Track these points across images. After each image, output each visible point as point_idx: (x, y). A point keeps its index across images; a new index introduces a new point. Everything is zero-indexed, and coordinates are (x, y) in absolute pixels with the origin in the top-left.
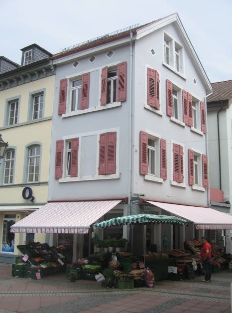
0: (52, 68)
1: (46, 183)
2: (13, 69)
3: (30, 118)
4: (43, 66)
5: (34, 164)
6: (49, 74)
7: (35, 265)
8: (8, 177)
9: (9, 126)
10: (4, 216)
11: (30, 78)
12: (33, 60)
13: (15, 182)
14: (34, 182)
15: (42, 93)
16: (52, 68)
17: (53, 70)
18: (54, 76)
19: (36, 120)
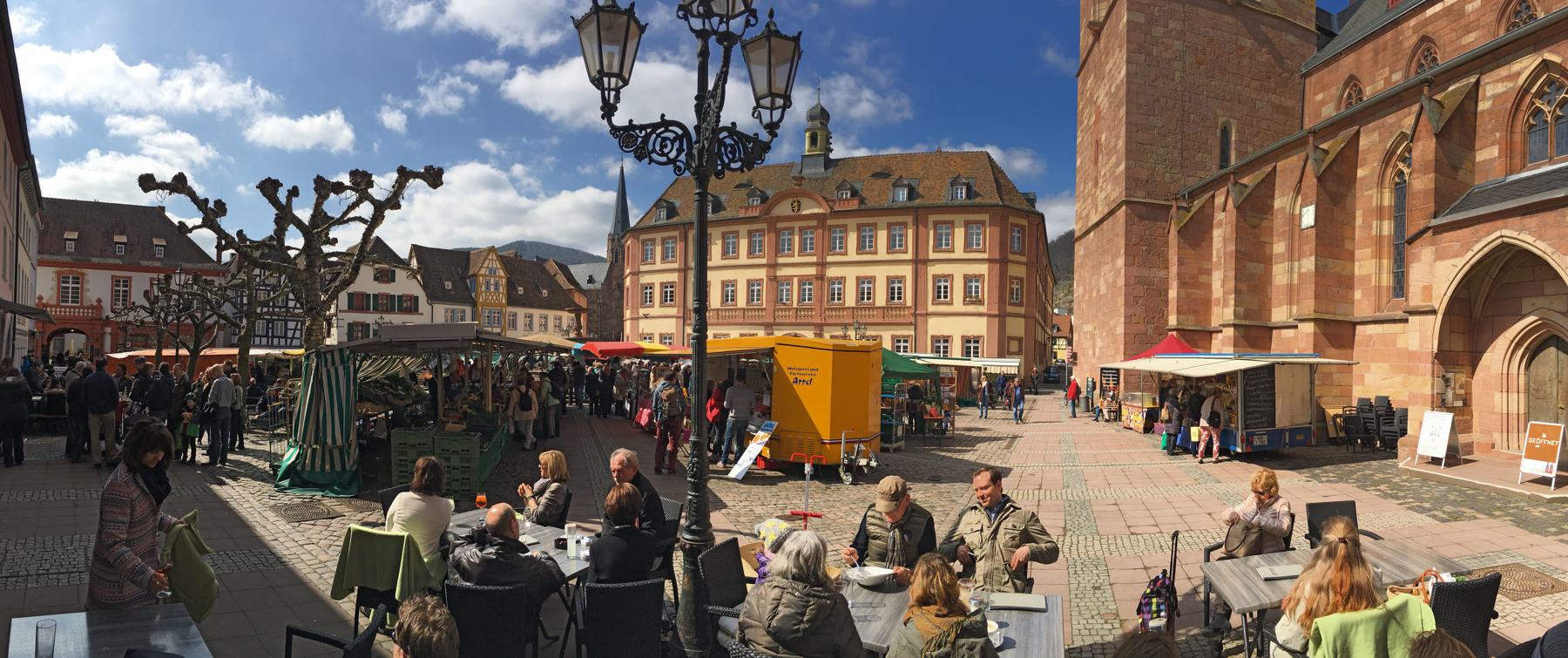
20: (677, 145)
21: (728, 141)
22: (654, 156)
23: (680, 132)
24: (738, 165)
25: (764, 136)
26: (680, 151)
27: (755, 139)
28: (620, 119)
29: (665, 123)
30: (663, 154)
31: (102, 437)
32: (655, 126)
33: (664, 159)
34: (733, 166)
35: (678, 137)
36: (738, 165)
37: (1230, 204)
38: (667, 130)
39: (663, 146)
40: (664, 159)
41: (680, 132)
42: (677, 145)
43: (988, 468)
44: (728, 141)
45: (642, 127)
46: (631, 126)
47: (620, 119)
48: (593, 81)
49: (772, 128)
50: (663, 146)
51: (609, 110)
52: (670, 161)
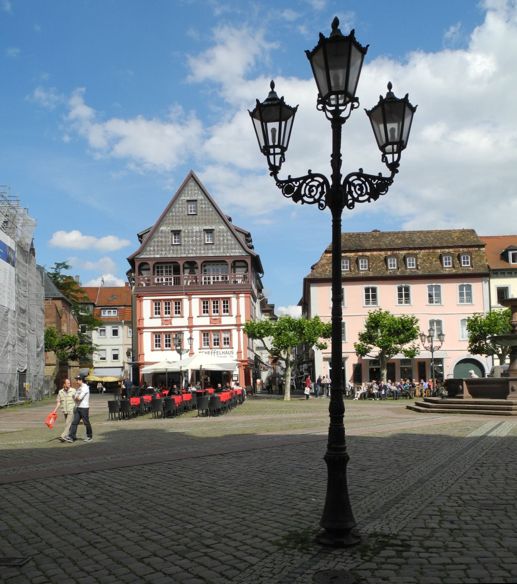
20: (320, 189)
21: (356, 182)
22: (305, 198)
23: (321, 180)
24: (366, 197)
25: (387, 173)
26: (322, 193)
27: (380, 177)
28: (282, 176)
29: (311, 176)
30: (311, 197)
31: (111, 458)
32: (305, 179)
33: (311, 200)
34: (361, 199)
35: (321, 185)
36: (366, 197)
37: (140, 456)
38: (313, 180)
39: (310, 191)
40: (311, 200)
41: (321, 180)
42: (320, 189)
43: (417, 397)
44: (356, 182)
45: (297, 180)
46: (290, 180)
47: (282, 176)
48: (262, 151)
49: (394, 167)
50: (310, 191)
51: (274, 170)
52: (315, 201)
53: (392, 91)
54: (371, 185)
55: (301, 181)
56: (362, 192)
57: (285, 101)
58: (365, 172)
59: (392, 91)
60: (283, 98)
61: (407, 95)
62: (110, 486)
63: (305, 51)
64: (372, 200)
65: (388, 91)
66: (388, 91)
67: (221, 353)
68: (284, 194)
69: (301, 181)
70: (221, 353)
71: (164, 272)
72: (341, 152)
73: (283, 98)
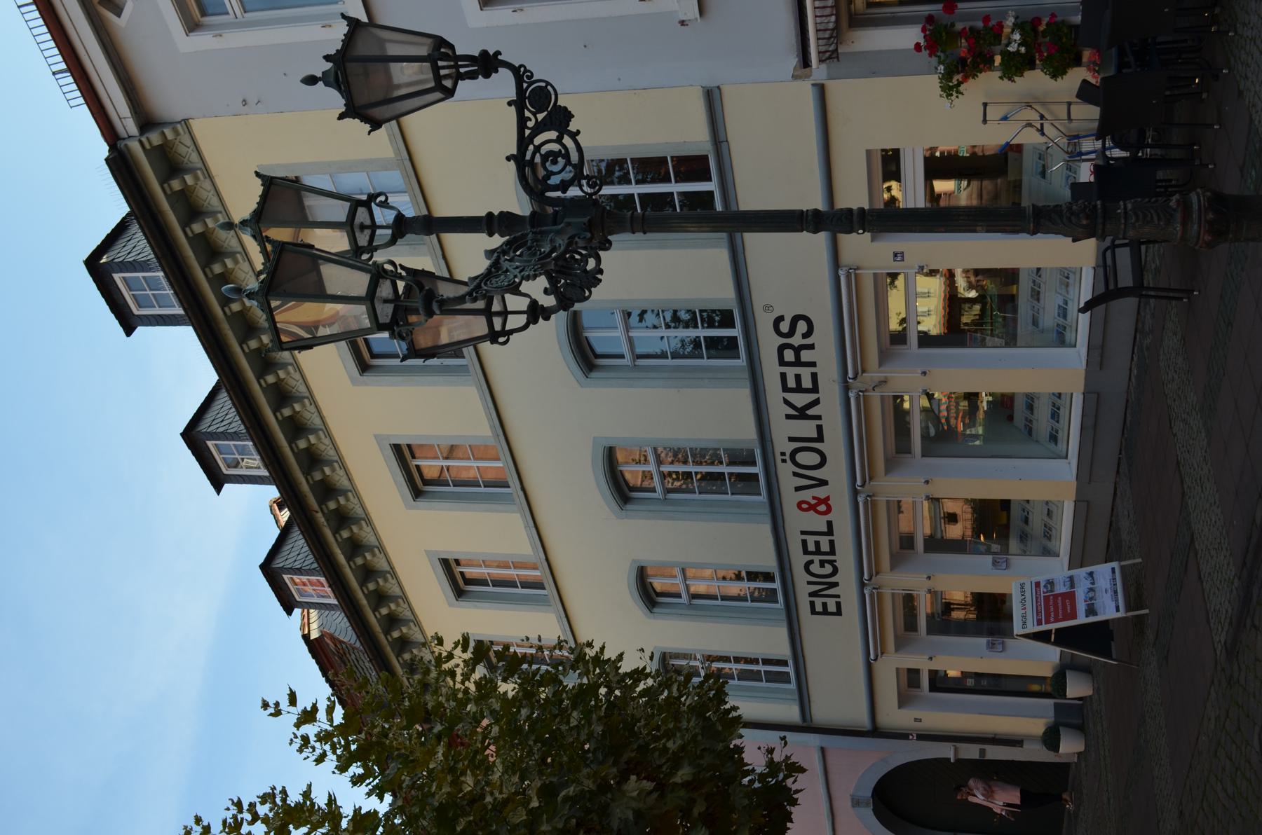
0: (155, 138)
1: (712, 99)
2: (140, 235)
3: (542, 602)
4: (382, 637)
5: (688, 475)
6: (194, 157)
7: (1122, 149)
8: (666, 179)
9: (550, 590)
10: (915, 691)
11: (297, 407)
12: (235, 436)
13: (782, 649)
14: (758, 469)
15: (448, 566)
16: (155, 138)
17: (312, 438)
18: (196, 125)
19: (549, 583)
36: (567, 140)
53: (319, 75)
54: (540, 128)
55: (527, 132)
56: (558, 154)
57: (333, 52)
58: (513, 150)
59: (319, 75)
60: (327, 58)
61: (341, 117)
62: (1035, 322)
63: (376, 436)
64: (573, 127)
65: (321, 84)
66: (321, 84)
67: (806, 429)
68: (548, 83)
69: (527, 132)
70: (806, 429)
71: (692, 333)
72: (483, 214)
73: (327, 58)
